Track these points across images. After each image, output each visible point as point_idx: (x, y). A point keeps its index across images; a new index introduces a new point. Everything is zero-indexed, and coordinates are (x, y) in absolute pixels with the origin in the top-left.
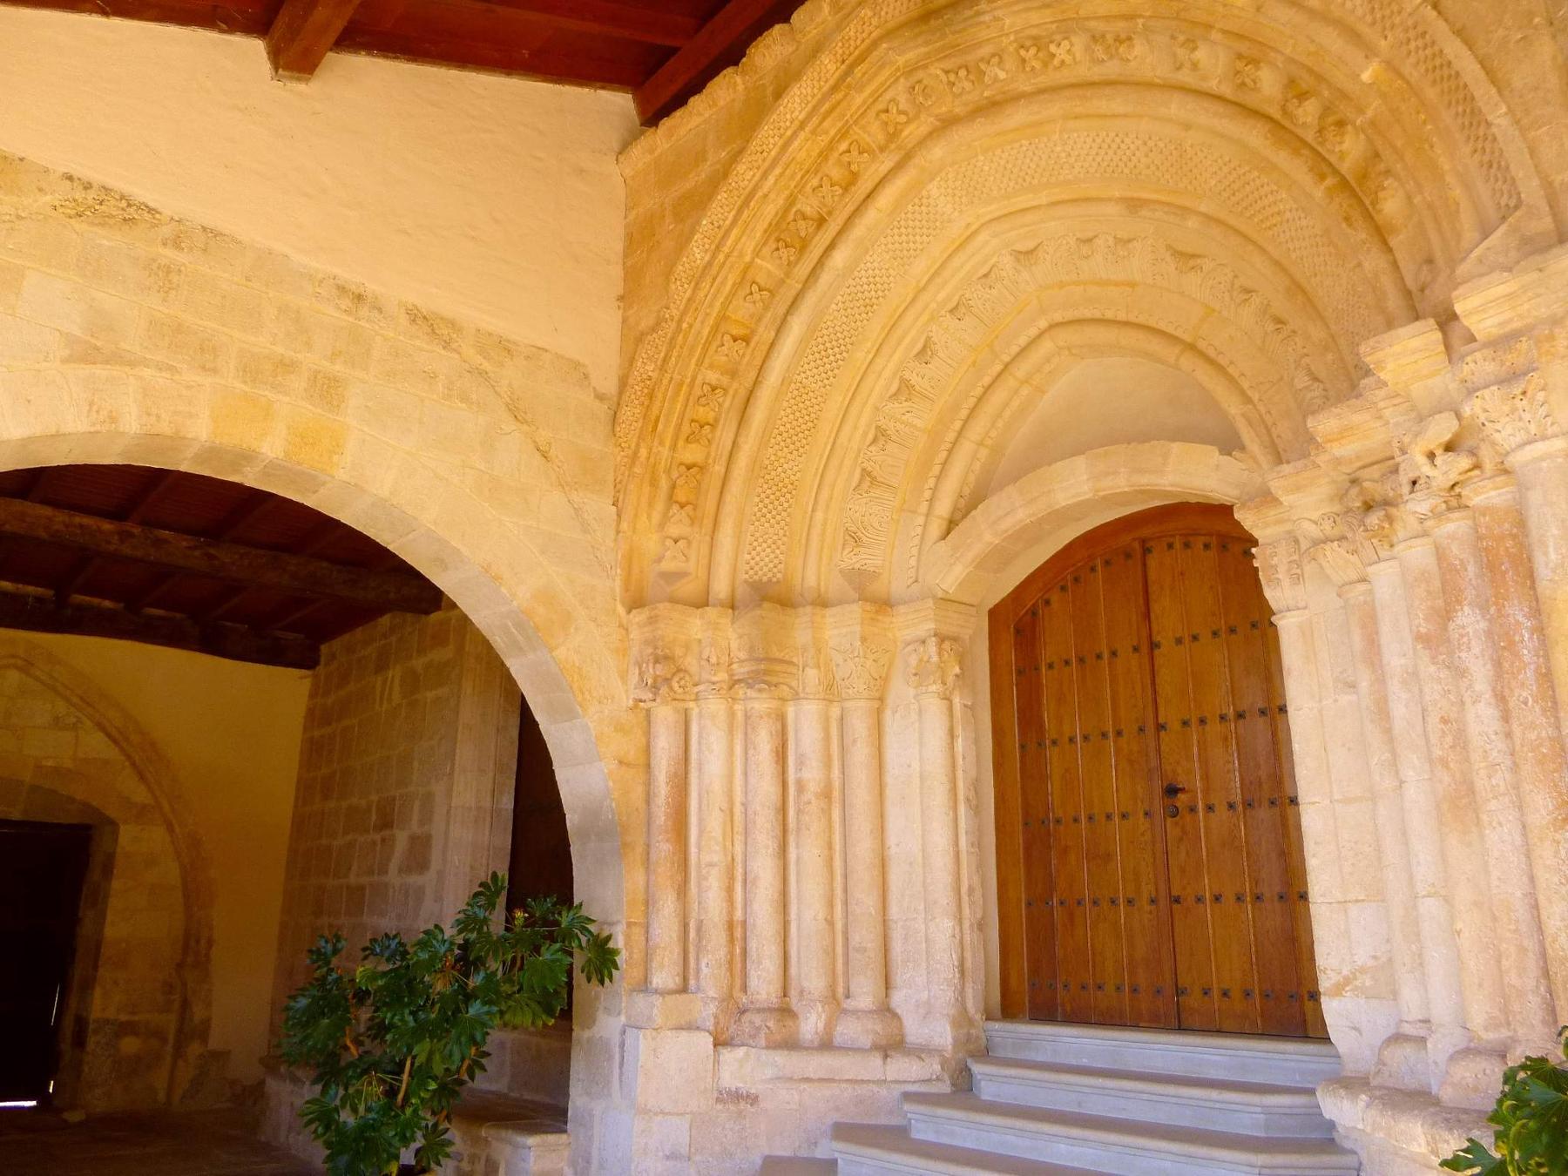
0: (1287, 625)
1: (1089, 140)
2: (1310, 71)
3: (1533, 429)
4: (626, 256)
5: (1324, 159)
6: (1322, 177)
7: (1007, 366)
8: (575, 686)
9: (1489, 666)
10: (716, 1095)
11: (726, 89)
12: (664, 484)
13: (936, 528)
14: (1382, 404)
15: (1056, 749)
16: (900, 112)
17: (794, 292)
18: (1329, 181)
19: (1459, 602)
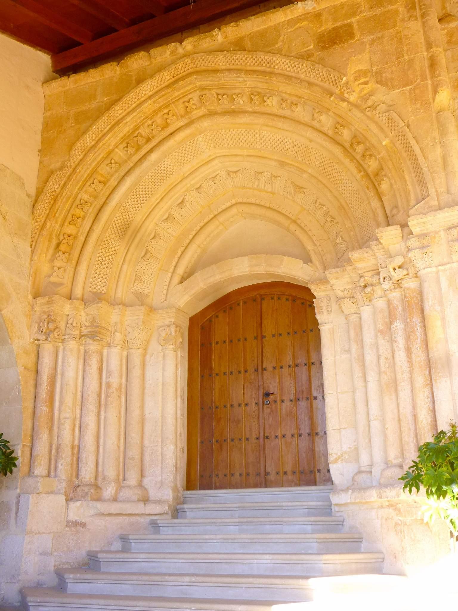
0: (325, 330)
1: (271, 136)
2: (363, 135)
3: (427, 263)
4: (43, 132)
5: (361, 165)
6: (360, 172)
7: (215, 216)
8: (9, 329)
9: (404, 339)
10: (66, 523)
11: (109, 72)
12: (54, 242)
13: (177, 279)
14: (376, 251)
15: (217, 378)
16: (194, 104)
17: (129, 167)
18: (362, 173)
19: (396, 318)
